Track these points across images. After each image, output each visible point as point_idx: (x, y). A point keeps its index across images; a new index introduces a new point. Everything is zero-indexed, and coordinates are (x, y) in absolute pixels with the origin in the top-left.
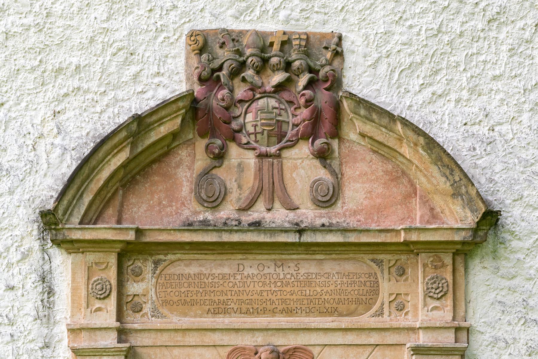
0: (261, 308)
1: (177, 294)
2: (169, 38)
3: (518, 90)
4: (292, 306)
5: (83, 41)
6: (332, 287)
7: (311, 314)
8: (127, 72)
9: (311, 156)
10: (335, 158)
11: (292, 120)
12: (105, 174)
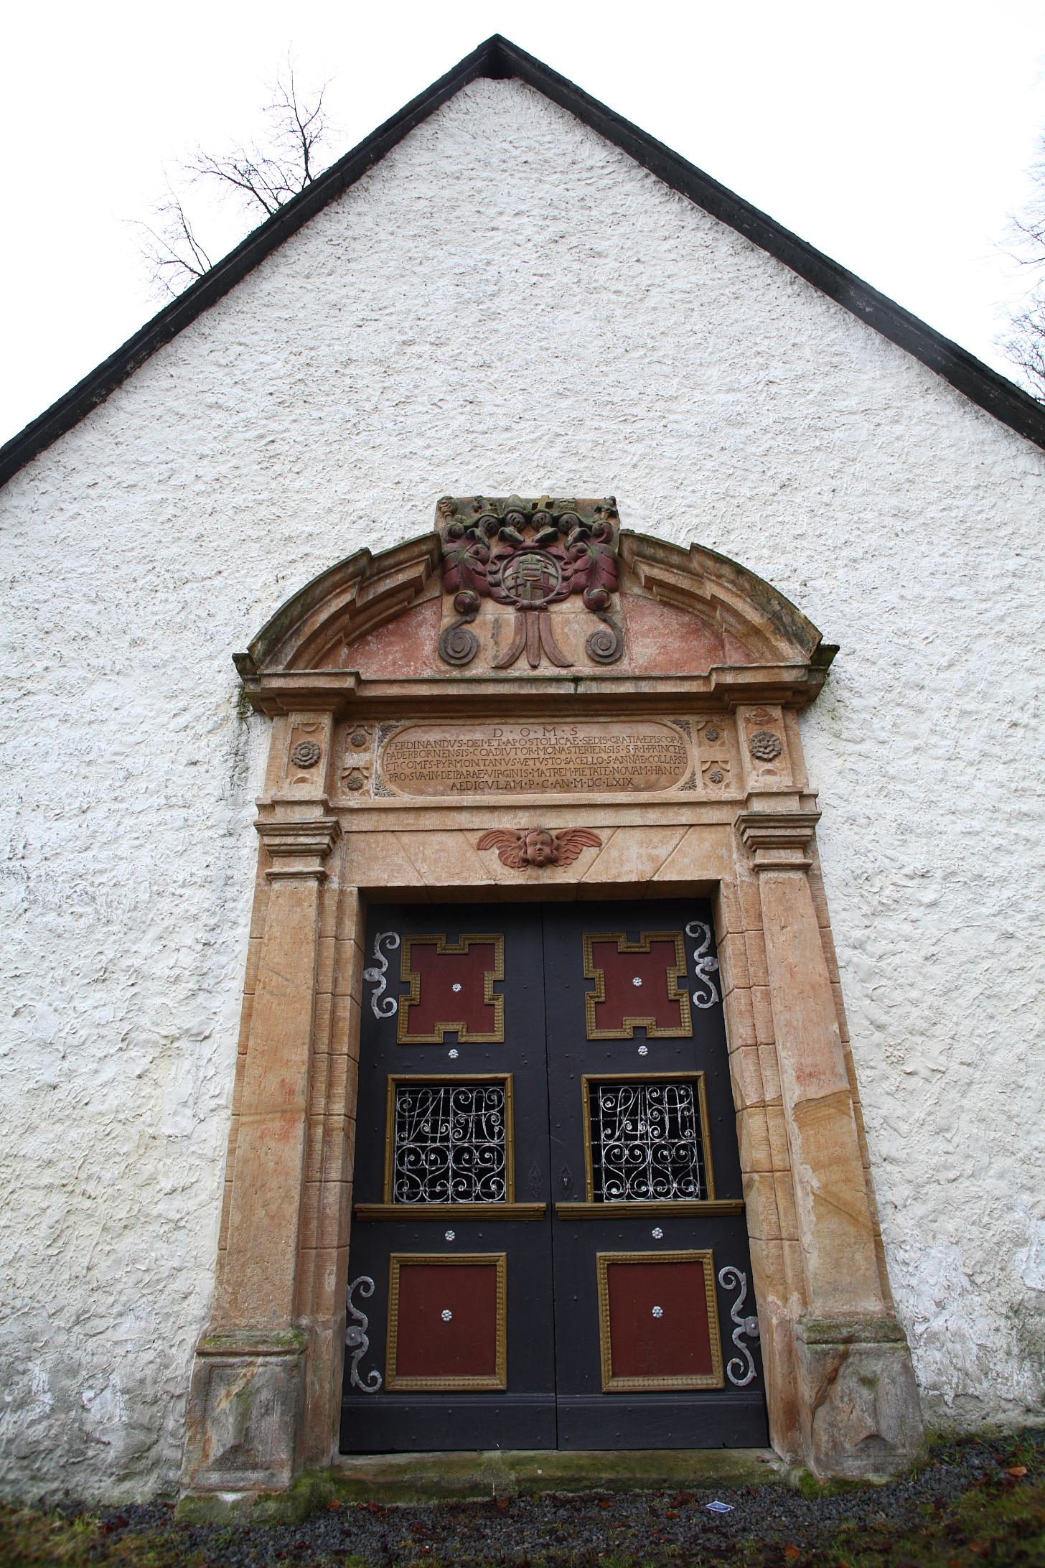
0: (525, 780)
1: (410, 765)
6: (623, 753)
8: (367, 539)
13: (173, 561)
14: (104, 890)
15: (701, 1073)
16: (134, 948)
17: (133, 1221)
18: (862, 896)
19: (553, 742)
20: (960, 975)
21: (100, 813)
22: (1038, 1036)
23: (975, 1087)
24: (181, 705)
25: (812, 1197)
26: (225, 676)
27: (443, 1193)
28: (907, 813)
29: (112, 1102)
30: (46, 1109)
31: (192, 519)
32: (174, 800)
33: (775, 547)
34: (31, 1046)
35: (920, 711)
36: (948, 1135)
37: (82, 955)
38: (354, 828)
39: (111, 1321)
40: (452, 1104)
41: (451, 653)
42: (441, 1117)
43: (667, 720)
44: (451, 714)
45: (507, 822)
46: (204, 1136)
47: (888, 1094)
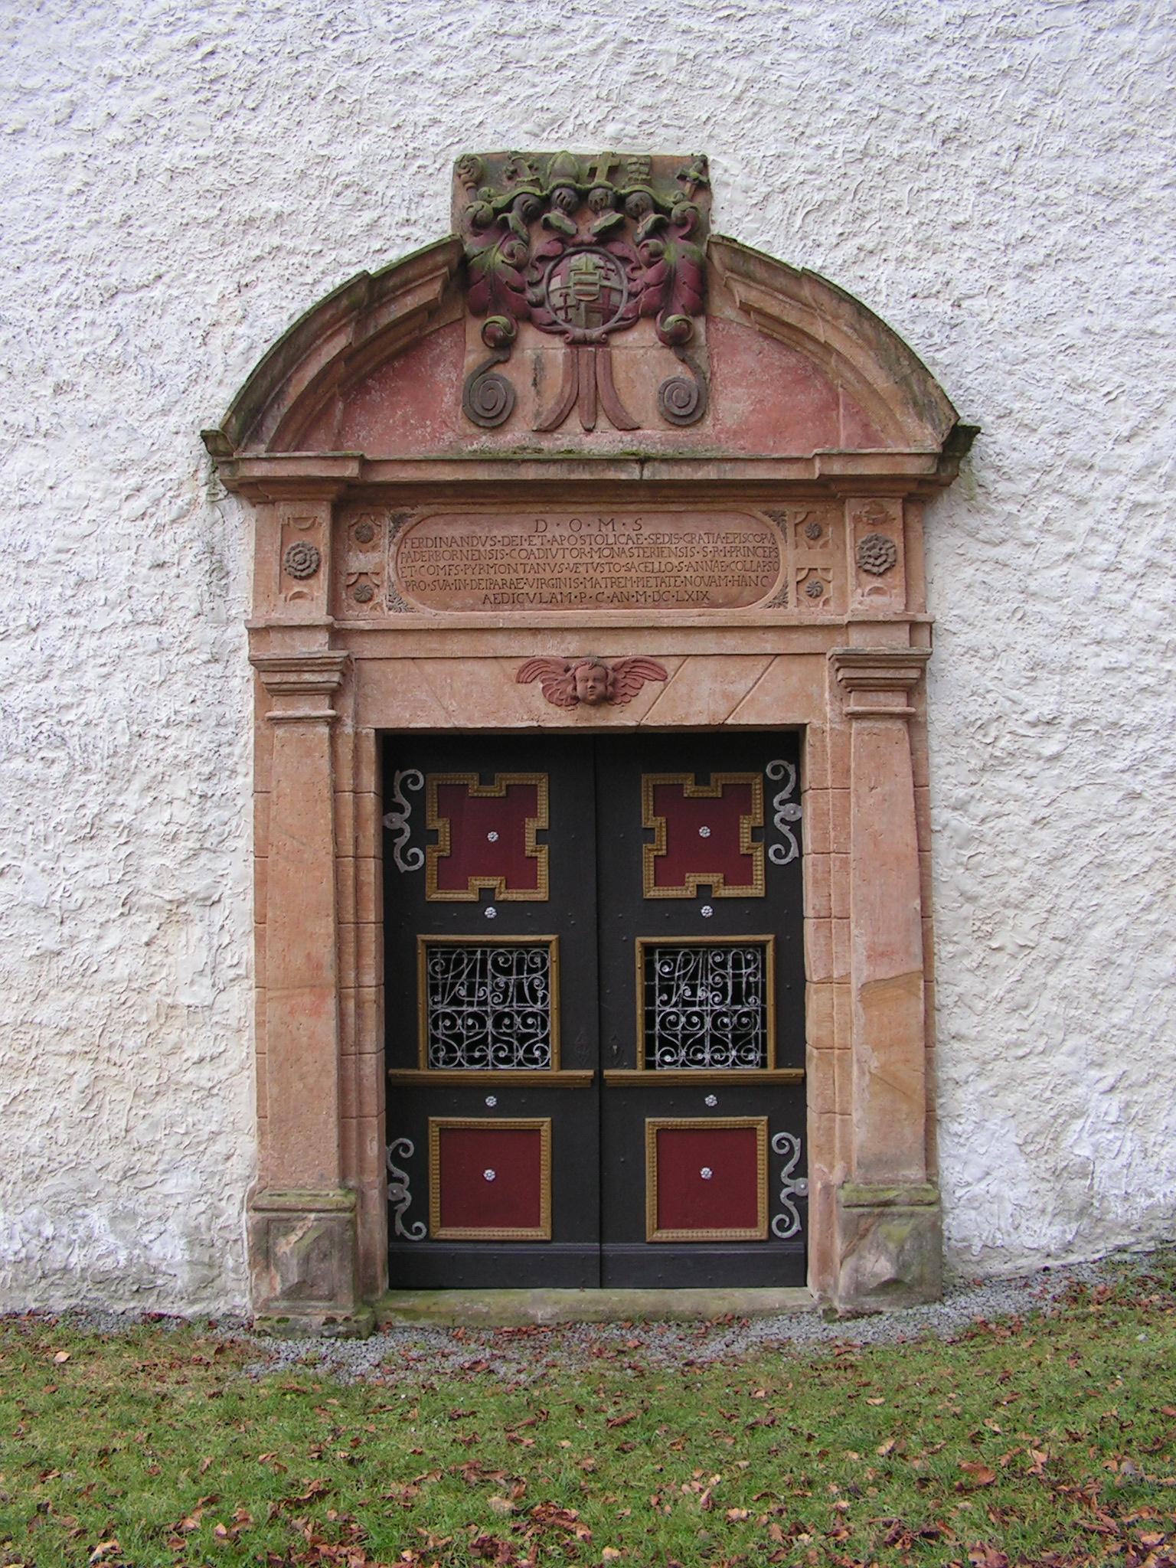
0: (575, 592)
1: (432, 570)
2: (425, 167)
3: (996, 246)
4: (631, 589)
5: (288, 177)
6: (698, 557)
7: (663, 604)
8: (358, 222)
9: (660, 344)
10: (699, 347)
11: (626, 286)
12: (312, 371)
13: (93, 259)
14: (76, 730)
15: (770, 937)
16: (120, 801)
17: (163, 1088)
18: (972, 747)
19: (611, 540)
21: (54, 631)
22: (1143, 909)
23: (1065, 963)
24: (133, 482)
25: (867, 1077)
26: (186, 441)
27: (483, 1058)
28: (1043, 642)
29: (122, 970)
30: (53, 976)
31: (113, 189)
32: (141, 616)
33: (922, 245)
34: (24, 910)
35: (1082, 502)
36: (1025, 1013)
37: (63, 808)
38: (367, 654)
39: (158, 1178)
40: (489, 966)
41: (481, 412)
42: (478, 980)
43: (757, 510)
45: (552, 649)
46: (226, 1007)
47: (968, 970)
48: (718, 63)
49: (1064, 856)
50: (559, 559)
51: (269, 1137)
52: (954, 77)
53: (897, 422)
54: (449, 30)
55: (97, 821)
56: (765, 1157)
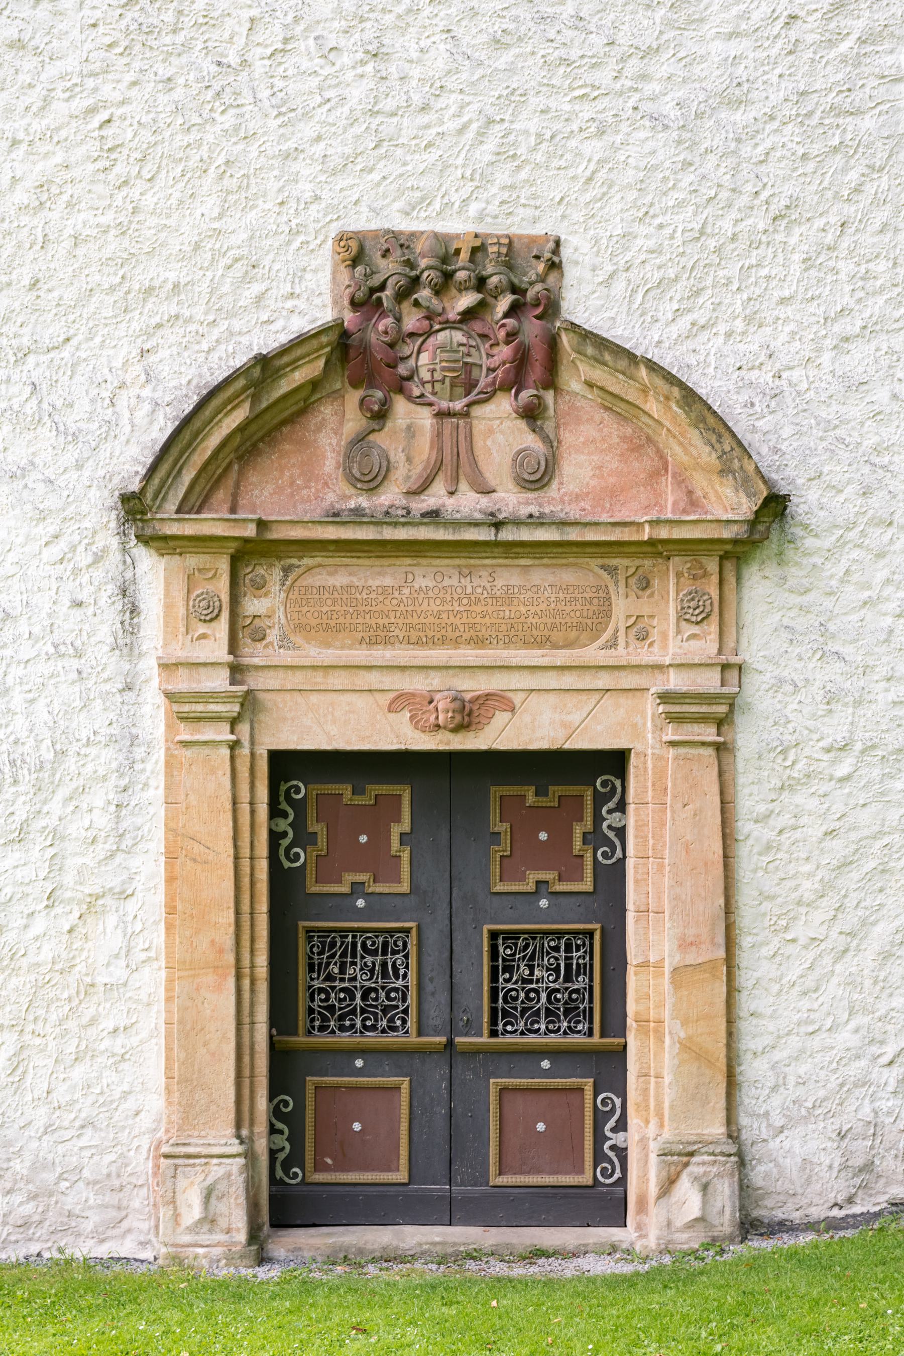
0: (438, 636)
2: (308, 242)
3: (817, 319)
4: (484, 633)
5: (184, 248)
6: (543, 607)
9: (514, 415)
10: (548, 418)
11: (486, 362)
12: (214, 440)
15: (597, 926)
16: (45, 810)
18: (774, 769)
19: (469, 590)
20: (857, 850)
24: (52, 529)
27: (353, 1026)
29: (46, 954)
35: (881, 555)
40: (359, 948)
41: (358, 475)
44: (359, 554)
45: (418, 684)
46: (138, 985)
47: (766, 958)
48: (573, 143)
49: (851, 863)
50: (425, 606)
51: (177, 1094)
52: (789, 154)
53: (716, 491)
54: (328, 106)
55: (25, 825)
56: (591, 1114)
